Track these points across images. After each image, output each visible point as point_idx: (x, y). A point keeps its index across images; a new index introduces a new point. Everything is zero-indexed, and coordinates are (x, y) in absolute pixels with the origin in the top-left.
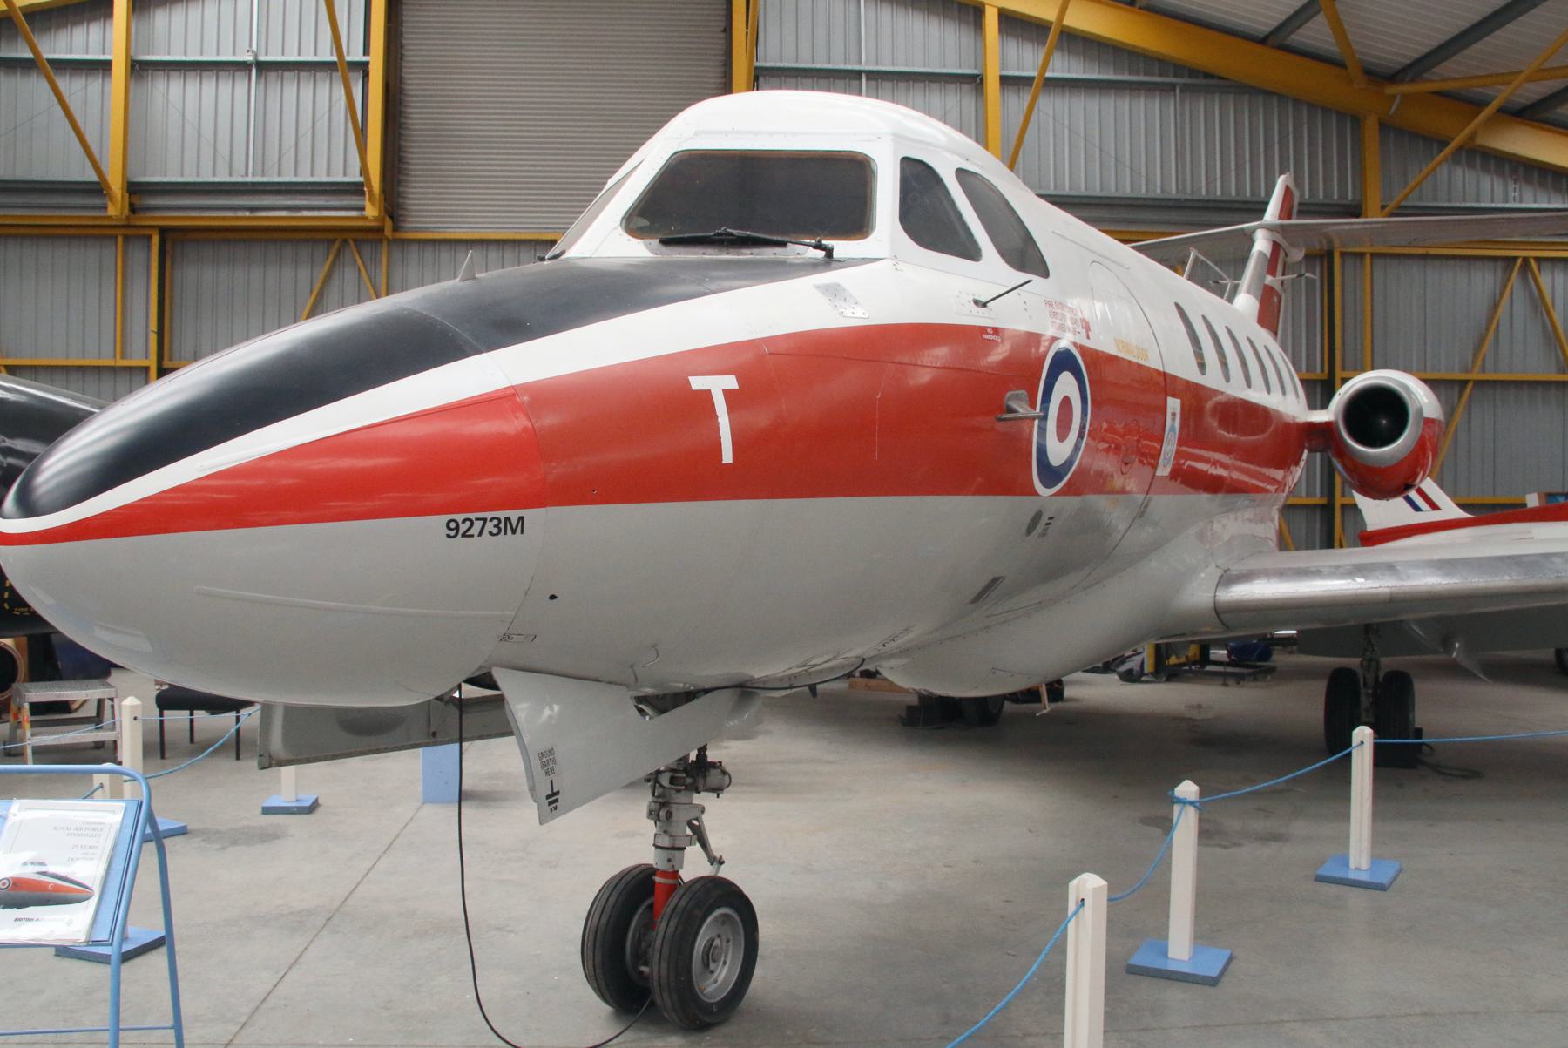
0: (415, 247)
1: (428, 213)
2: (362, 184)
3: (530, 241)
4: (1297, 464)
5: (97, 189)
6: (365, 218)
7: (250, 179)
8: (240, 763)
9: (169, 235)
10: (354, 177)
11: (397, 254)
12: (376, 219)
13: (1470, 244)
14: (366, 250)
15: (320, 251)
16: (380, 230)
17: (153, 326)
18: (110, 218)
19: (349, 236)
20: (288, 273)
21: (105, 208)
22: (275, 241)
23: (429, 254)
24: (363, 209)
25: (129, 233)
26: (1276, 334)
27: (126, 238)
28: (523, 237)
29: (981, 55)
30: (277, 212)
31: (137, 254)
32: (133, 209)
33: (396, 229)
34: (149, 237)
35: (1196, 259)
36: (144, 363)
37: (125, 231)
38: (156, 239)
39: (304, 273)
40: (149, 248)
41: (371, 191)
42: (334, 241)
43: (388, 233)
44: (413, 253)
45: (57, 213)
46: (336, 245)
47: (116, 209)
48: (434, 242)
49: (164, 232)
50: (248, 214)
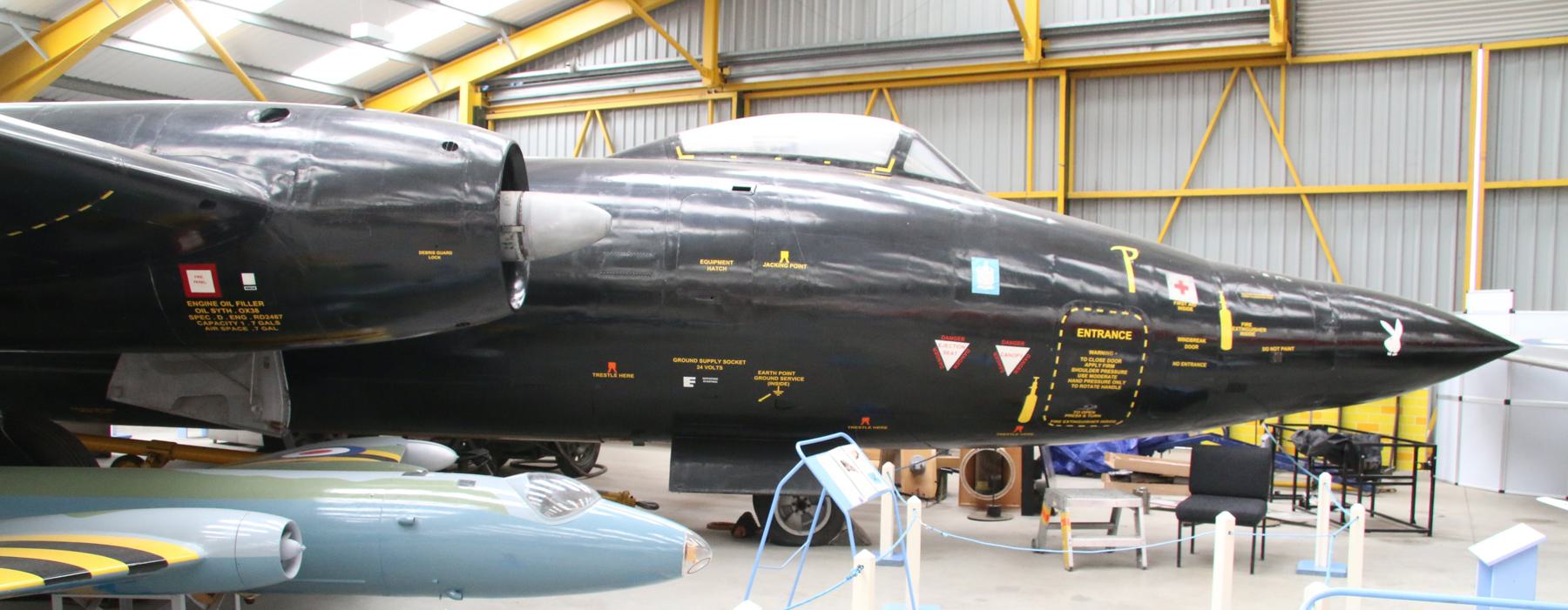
1: (1323, 40)
2: (1267, 12)
3: (1439, 57)
5: (1015, 38)
6: (1269, 45)
7: (1153, 17)
8: (1256, 577)
9: (1078, 77)
10: (1011, 26)
11: (1294, 79)
12: (1279, 46)
14: (1263, 76)
15: (1216, 81)
16: (1282, 56)
17: (1061, 160)
18: (1024, 63)
19: (1247, 65)
21: (1021, 54)
22: (1128, 77)
23: (1327, 76)
24: (1267, 36)
25: (1040, 76)
27: (1036, 80)
28: (1426, 52)
30: (1176, 46)
31: (1045, 94)
32: (1044, 54)
33: (1294, 55)
34: (1057, 78)
36: (1053, 195)
37: (1037, 75)
38: (1063, 80)
39: (1200, 103)
40: (1056, 87)
41: (1276, 19)
42: (1232, 70)
43: (1288, 58)
44: (1310, 76)
45: (909, 68)
46: (1234, 73)
47: (1031, 55)
48: (1333, 64)
49: (1070, 71)
50: (1149, 50)
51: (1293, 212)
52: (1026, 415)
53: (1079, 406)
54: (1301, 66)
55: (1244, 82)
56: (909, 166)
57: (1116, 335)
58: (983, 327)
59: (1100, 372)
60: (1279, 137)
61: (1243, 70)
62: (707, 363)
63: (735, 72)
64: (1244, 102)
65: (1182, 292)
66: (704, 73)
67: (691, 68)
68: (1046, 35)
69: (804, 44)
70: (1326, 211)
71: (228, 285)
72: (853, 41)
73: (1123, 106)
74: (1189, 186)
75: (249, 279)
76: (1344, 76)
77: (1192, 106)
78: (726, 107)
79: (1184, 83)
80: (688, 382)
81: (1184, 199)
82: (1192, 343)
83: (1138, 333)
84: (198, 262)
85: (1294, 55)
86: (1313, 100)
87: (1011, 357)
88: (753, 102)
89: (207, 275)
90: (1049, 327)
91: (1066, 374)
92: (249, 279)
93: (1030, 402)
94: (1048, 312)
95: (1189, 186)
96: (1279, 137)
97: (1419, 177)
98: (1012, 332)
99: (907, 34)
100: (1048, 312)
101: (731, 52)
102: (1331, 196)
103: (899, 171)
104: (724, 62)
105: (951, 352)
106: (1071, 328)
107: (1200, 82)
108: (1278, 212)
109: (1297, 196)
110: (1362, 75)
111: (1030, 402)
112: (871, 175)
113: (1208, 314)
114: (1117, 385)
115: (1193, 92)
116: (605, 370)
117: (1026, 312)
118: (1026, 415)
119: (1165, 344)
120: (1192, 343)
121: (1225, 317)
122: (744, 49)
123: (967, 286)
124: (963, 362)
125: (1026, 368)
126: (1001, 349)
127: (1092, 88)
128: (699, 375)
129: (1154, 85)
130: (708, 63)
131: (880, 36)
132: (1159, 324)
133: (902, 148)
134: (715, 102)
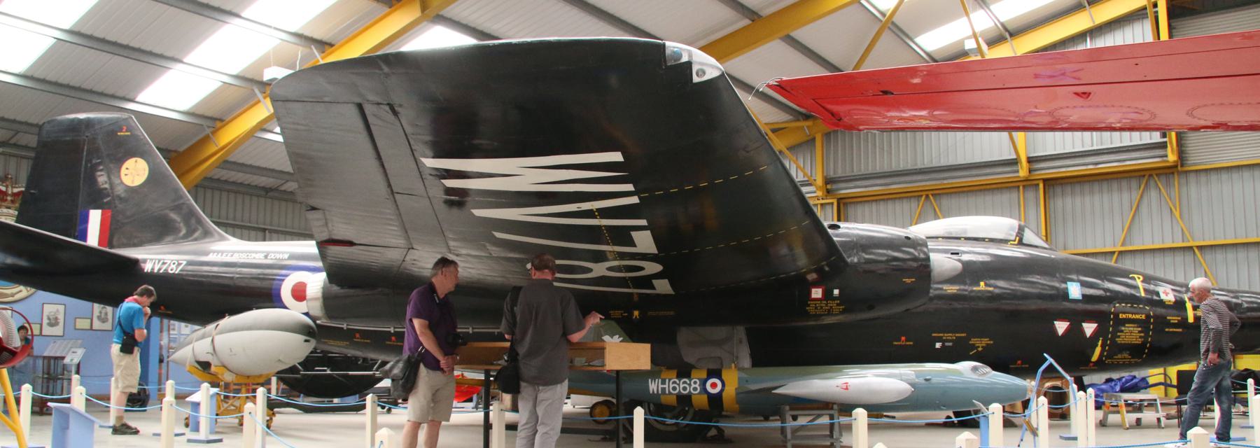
0: (1192, 175)
4: (135, 262)
5: (1014, 162)
7: (1095, 148)
9: (1050, 183)
11: (1183, 181)
13: (953, 121)
14: (1163, 178)
15: (1134, 183)
19: (1154, 173)
20: (1116, 196)
23: (1203, 178)
25: (1028, 184)
26: (287, 276)
29: (1123, 419)
31: (1031, 194)
32: (1030, 171)
35: (1192, 373)
38: (1041, 186)
44: (1192, 178)
47: (1023, 172)
48: (1206, 170)
49: (1045, 180)
51: (1189, 257)
52: (1095, 358)
53: (1121, 352)
54: (1186, 172)
55: (1152, 183)
56: (1025, 241)
57: (1138, 317)
58: (1077, 316)
59: (1131, 335)
60: (1177, 214)
61: (1151, 176)
62: (949, 336)
63: (834, 186)
64: (1153, 194)
65: (1167, 295)
66: (818, 188)
67: (810, 185)
68: (1031, 160)
69: (878, 170)
70: (1209, 256)
71: (827, 295)
72: (909, 167)
73: (1078, 200)
74: (1123, 245)
75: (836, 292)
76: (1214, 177)
77: (1120, 199)
78: (828, 209)
79: (1115, 185)
80: (938, 345)
81: (1121, 252)
82: (1174, 319)
83: (1148, 316)
84: (816, 284)
85: (1182, 166)
86: (1195, 191)
87: (1089, 328)
88: (845, 204)
89: (814, 290)
90: (1108, 313)
91: (1115, 335)
92: (836, 292)
93: (1098, 350)
94: (1104, 307)
95: (1123, 245)
96: (1177, 214)
97: (231, 215)
98: (1090, 317)
99: (952, 161)
100: (1104, 307)
101: (832, 174)
102: (1212, 246)
103: (1021, 243)
104: (828, 181)
105: (1061, 327)
106: (1116, 315)
107: (1124, 183)
108: (1179, 258)
109: (1191, 248)
110: (1225, 176)
111: (1098, 350)
112: (1008, 246)
113: (1179, 305)
114: (1139, 341)
115: (1120, 190)
116: (899, 340)
117: (1092, 308)
118: (1095, 358)
119: (1161, 322)
120: (1174, 319)
121: (1189, 305)
122: (840, 173)
123: (1067, 294)
124: (1067, 331)
125: (1096, 334)
126: (1095, 325)
127: (1059, 190)
128: (943, 341)
129: (1096, 186)
130: (820, 181)
131: (927, 163)
132: (1160, 311)
133: (1021, 230)
134: (822, 205)
